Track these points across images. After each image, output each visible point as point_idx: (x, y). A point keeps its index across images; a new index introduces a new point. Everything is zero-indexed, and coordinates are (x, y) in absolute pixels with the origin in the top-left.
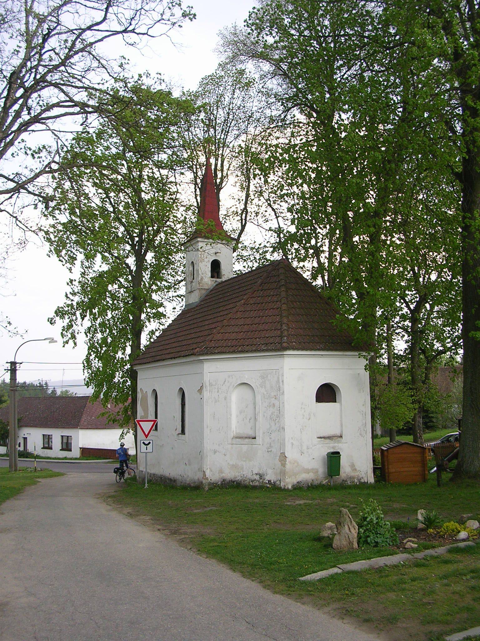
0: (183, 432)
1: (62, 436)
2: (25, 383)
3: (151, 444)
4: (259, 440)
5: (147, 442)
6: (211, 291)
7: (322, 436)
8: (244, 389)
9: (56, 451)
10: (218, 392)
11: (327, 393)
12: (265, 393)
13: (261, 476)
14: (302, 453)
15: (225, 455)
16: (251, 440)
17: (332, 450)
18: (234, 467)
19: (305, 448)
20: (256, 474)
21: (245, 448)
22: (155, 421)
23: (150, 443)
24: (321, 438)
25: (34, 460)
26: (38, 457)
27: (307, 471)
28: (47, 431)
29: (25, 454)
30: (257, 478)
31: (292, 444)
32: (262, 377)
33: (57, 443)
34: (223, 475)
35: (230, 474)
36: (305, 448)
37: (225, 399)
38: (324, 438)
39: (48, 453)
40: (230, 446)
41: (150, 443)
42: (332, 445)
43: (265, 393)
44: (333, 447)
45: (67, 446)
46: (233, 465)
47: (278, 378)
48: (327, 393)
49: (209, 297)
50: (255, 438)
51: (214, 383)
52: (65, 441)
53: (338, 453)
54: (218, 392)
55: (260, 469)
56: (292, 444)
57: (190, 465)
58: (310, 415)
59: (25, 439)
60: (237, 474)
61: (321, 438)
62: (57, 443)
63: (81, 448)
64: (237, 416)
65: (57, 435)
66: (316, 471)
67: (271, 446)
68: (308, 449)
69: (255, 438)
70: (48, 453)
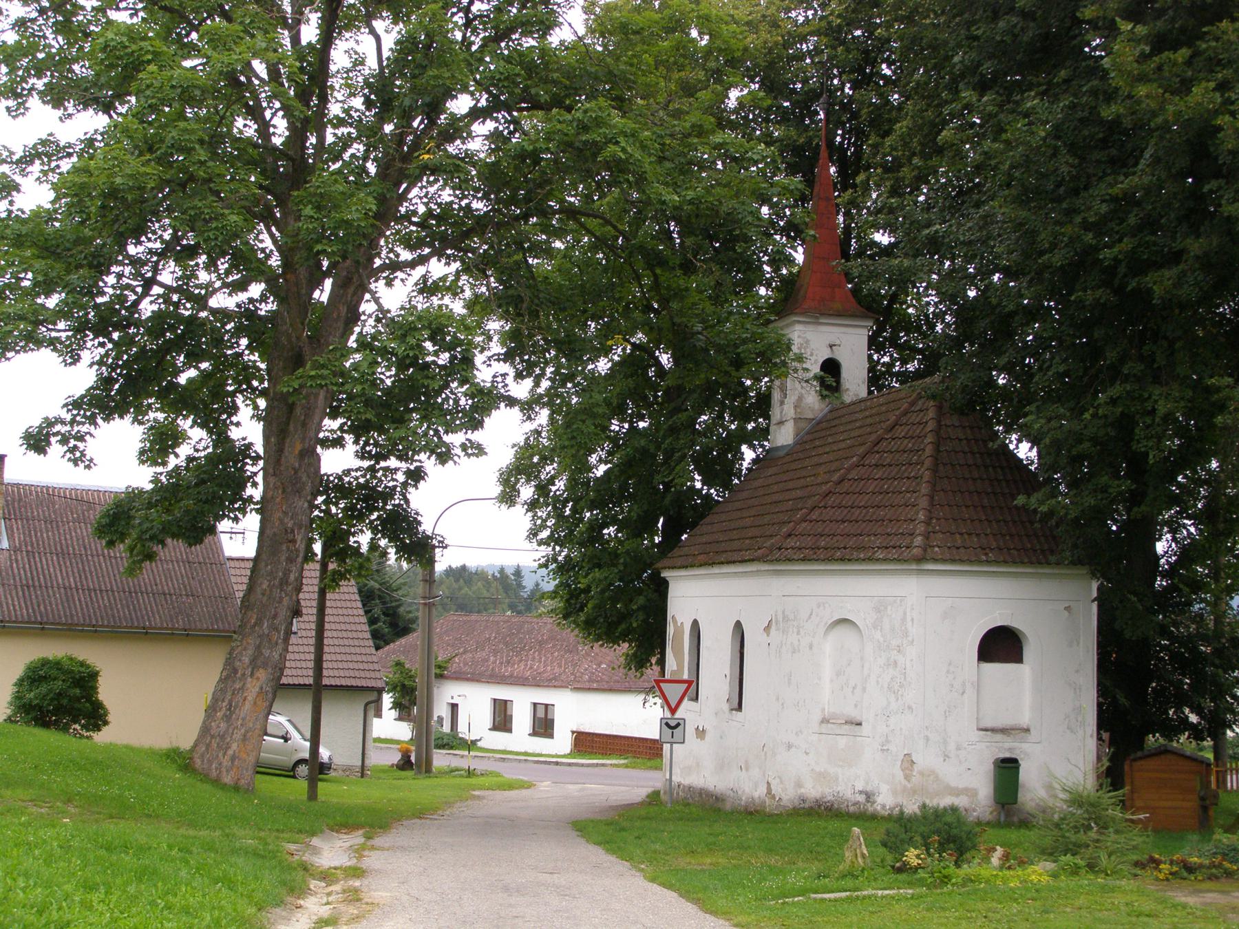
0: (740, 707)
1: (535, 705)
2: (464, 568)
3: (681, 728)
4: (866, 729)
5: (673, 723)
6: (819, 423)
7: (989, 725)
8: (841, 631)
9: (520, 738)
10: (798, 633)
11: (1001, 645)
12: (881, 640)
13: (869, 796)
14: (946, 757)
15: (807, 753)
16: (853, 727)
17: (1007, 755)
18: (821, 776)
19: (952, 747)
20: (861, 792)
21: (842, 742)
22: (689, 683)
23: (678, 725)
24: (986, 730)
25: (466, 753)
26: (471, 745)
27: (957, 792)
28: (503, 693)
29: (453, 742)
30: (862, 798)
31: (927, 739)
32: (877, 610)
33: (522, 718)
34: (803, 790)
35: (813, 790)
36: (952, 747)
37: (811, 648)
38: (993, 730)
39: (498, 740)
40: (815, 737)
41: (678, 725)
42: (1007, 745)
43: (881, 640)
44: (1010, 749)
45: (543, 725)
46: (820, 774)
47: (905, 613)
48: (1001, 645)
49: (817, 435)
50: (860, 724)
51: (791, 617)
52: (541, 714)
53: (1015, 761)
54: (798, 633)
55: (867, 783)
56: (927, 739)
57: (747, 770)
58: (964, 684)
59: (454, 707)
60: (827, 791)
61: (986, 730)
62: (522, 718)
63: (573, 732)
64: (832, 681)
65: (522, 702)
66: (970, 792)
67: (888, 741)
68: (958, 748)
69: (860, 724)
70: (498, 740)
